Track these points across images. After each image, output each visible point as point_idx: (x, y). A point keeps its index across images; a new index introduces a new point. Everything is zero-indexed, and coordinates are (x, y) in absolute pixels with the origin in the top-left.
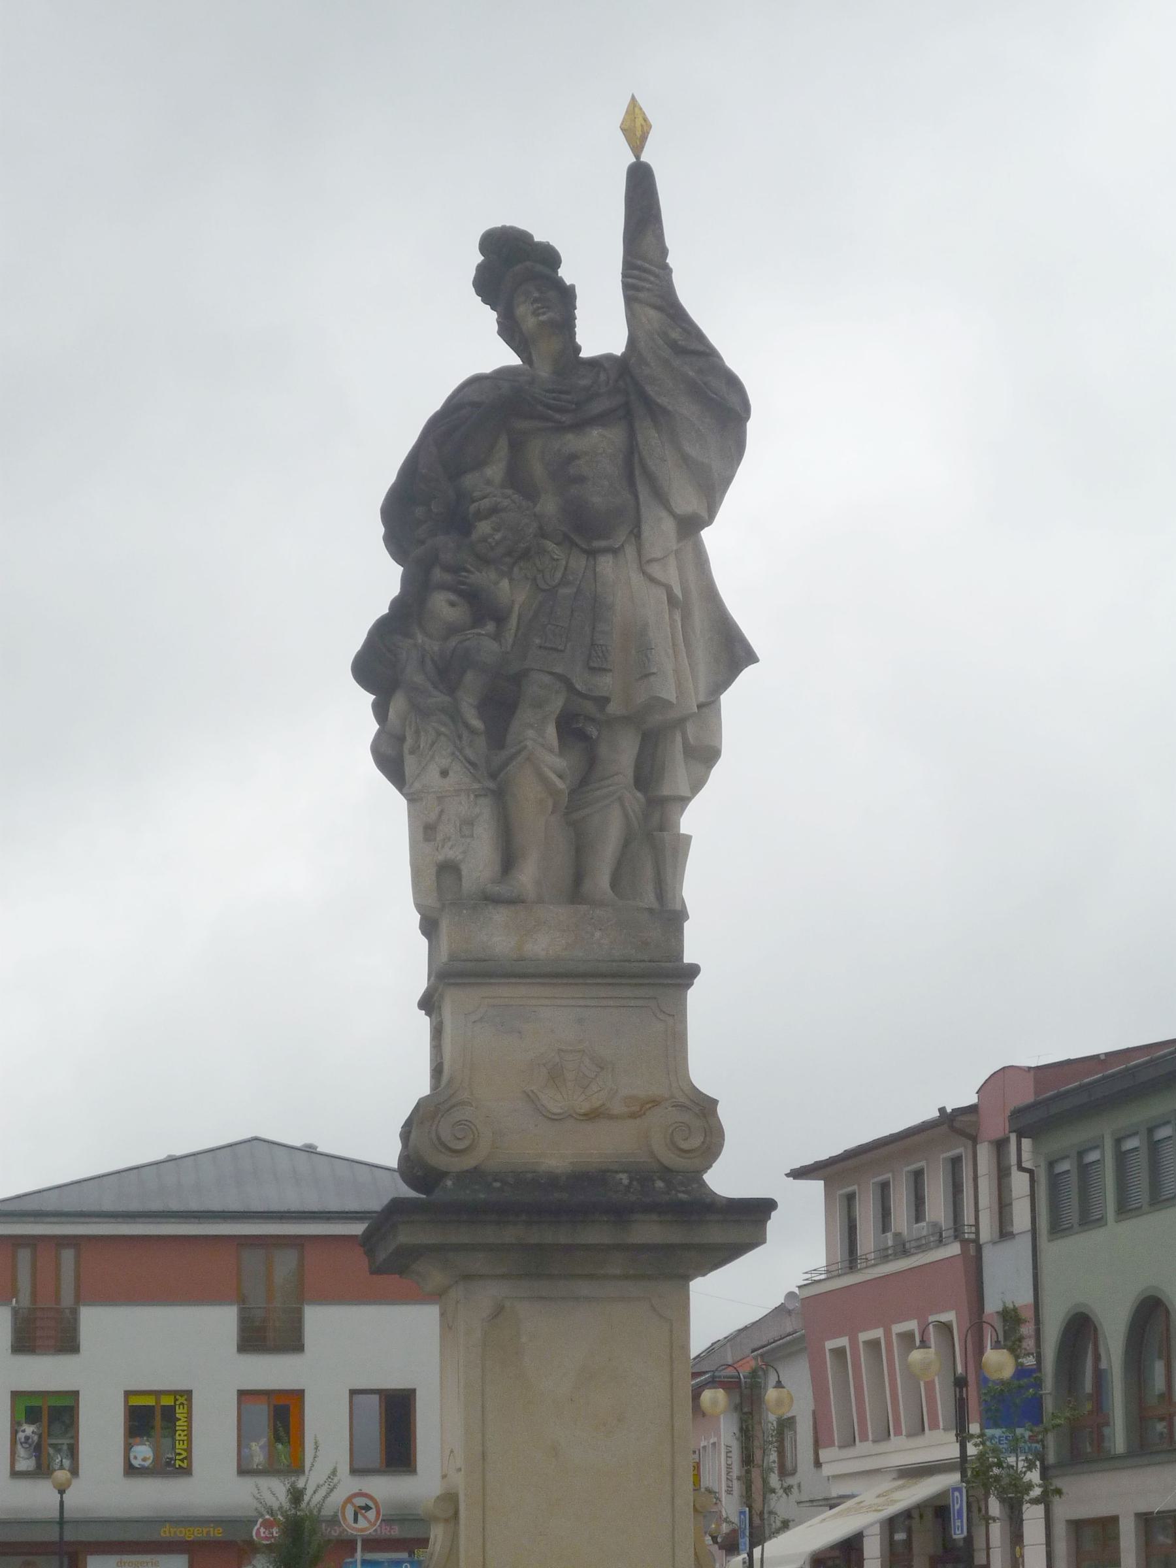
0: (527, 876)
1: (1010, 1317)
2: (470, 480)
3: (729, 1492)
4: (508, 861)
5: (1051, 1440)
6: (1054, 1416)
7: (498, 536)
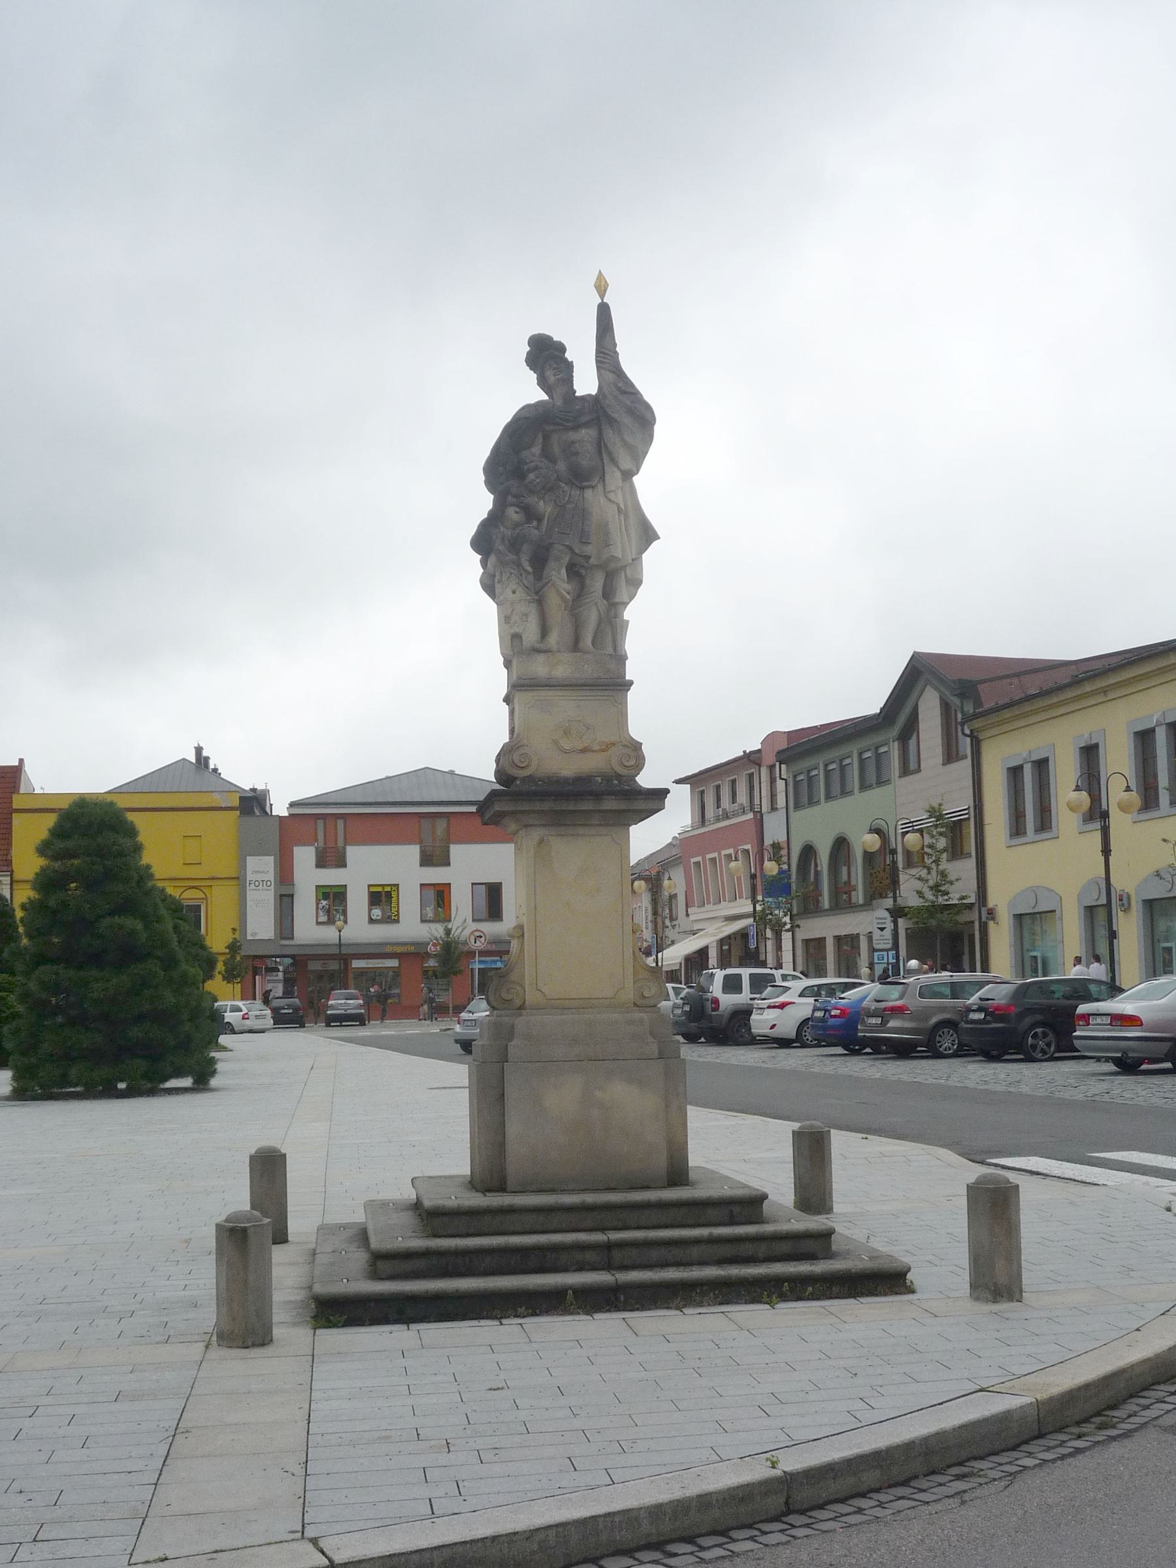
0: (553, 640)
1: (776, 847)
2: (524, 454)
3: (647, 928)
4: (544, 632)
5: (794, 902)
6: (797, 892)
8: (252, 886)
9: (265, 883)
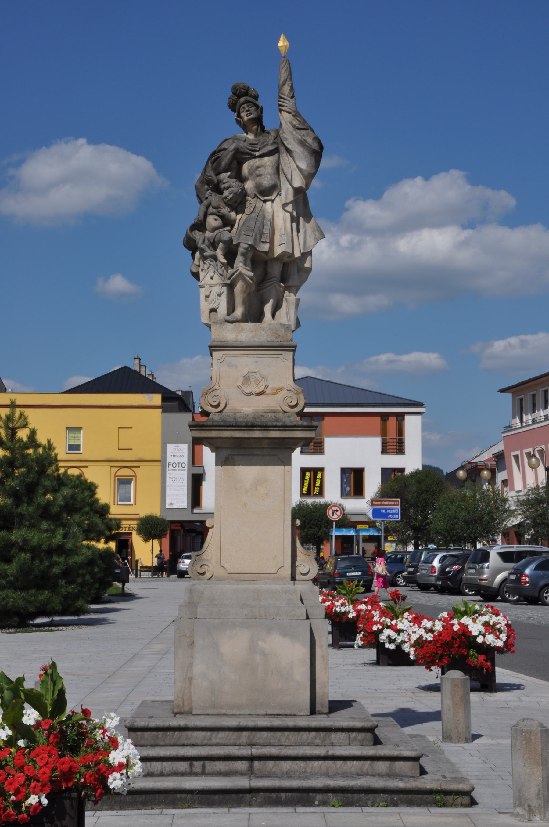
7: (231, 196)
8: (171, 467)
9: (180, 464)
